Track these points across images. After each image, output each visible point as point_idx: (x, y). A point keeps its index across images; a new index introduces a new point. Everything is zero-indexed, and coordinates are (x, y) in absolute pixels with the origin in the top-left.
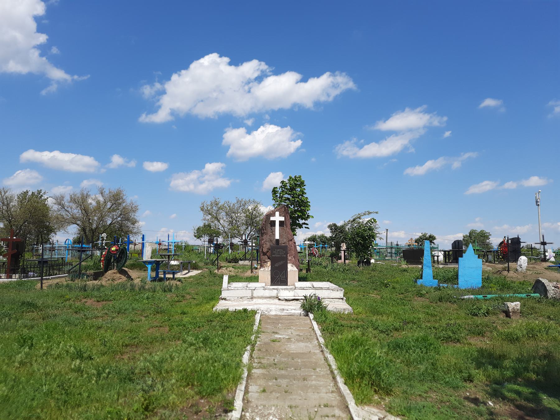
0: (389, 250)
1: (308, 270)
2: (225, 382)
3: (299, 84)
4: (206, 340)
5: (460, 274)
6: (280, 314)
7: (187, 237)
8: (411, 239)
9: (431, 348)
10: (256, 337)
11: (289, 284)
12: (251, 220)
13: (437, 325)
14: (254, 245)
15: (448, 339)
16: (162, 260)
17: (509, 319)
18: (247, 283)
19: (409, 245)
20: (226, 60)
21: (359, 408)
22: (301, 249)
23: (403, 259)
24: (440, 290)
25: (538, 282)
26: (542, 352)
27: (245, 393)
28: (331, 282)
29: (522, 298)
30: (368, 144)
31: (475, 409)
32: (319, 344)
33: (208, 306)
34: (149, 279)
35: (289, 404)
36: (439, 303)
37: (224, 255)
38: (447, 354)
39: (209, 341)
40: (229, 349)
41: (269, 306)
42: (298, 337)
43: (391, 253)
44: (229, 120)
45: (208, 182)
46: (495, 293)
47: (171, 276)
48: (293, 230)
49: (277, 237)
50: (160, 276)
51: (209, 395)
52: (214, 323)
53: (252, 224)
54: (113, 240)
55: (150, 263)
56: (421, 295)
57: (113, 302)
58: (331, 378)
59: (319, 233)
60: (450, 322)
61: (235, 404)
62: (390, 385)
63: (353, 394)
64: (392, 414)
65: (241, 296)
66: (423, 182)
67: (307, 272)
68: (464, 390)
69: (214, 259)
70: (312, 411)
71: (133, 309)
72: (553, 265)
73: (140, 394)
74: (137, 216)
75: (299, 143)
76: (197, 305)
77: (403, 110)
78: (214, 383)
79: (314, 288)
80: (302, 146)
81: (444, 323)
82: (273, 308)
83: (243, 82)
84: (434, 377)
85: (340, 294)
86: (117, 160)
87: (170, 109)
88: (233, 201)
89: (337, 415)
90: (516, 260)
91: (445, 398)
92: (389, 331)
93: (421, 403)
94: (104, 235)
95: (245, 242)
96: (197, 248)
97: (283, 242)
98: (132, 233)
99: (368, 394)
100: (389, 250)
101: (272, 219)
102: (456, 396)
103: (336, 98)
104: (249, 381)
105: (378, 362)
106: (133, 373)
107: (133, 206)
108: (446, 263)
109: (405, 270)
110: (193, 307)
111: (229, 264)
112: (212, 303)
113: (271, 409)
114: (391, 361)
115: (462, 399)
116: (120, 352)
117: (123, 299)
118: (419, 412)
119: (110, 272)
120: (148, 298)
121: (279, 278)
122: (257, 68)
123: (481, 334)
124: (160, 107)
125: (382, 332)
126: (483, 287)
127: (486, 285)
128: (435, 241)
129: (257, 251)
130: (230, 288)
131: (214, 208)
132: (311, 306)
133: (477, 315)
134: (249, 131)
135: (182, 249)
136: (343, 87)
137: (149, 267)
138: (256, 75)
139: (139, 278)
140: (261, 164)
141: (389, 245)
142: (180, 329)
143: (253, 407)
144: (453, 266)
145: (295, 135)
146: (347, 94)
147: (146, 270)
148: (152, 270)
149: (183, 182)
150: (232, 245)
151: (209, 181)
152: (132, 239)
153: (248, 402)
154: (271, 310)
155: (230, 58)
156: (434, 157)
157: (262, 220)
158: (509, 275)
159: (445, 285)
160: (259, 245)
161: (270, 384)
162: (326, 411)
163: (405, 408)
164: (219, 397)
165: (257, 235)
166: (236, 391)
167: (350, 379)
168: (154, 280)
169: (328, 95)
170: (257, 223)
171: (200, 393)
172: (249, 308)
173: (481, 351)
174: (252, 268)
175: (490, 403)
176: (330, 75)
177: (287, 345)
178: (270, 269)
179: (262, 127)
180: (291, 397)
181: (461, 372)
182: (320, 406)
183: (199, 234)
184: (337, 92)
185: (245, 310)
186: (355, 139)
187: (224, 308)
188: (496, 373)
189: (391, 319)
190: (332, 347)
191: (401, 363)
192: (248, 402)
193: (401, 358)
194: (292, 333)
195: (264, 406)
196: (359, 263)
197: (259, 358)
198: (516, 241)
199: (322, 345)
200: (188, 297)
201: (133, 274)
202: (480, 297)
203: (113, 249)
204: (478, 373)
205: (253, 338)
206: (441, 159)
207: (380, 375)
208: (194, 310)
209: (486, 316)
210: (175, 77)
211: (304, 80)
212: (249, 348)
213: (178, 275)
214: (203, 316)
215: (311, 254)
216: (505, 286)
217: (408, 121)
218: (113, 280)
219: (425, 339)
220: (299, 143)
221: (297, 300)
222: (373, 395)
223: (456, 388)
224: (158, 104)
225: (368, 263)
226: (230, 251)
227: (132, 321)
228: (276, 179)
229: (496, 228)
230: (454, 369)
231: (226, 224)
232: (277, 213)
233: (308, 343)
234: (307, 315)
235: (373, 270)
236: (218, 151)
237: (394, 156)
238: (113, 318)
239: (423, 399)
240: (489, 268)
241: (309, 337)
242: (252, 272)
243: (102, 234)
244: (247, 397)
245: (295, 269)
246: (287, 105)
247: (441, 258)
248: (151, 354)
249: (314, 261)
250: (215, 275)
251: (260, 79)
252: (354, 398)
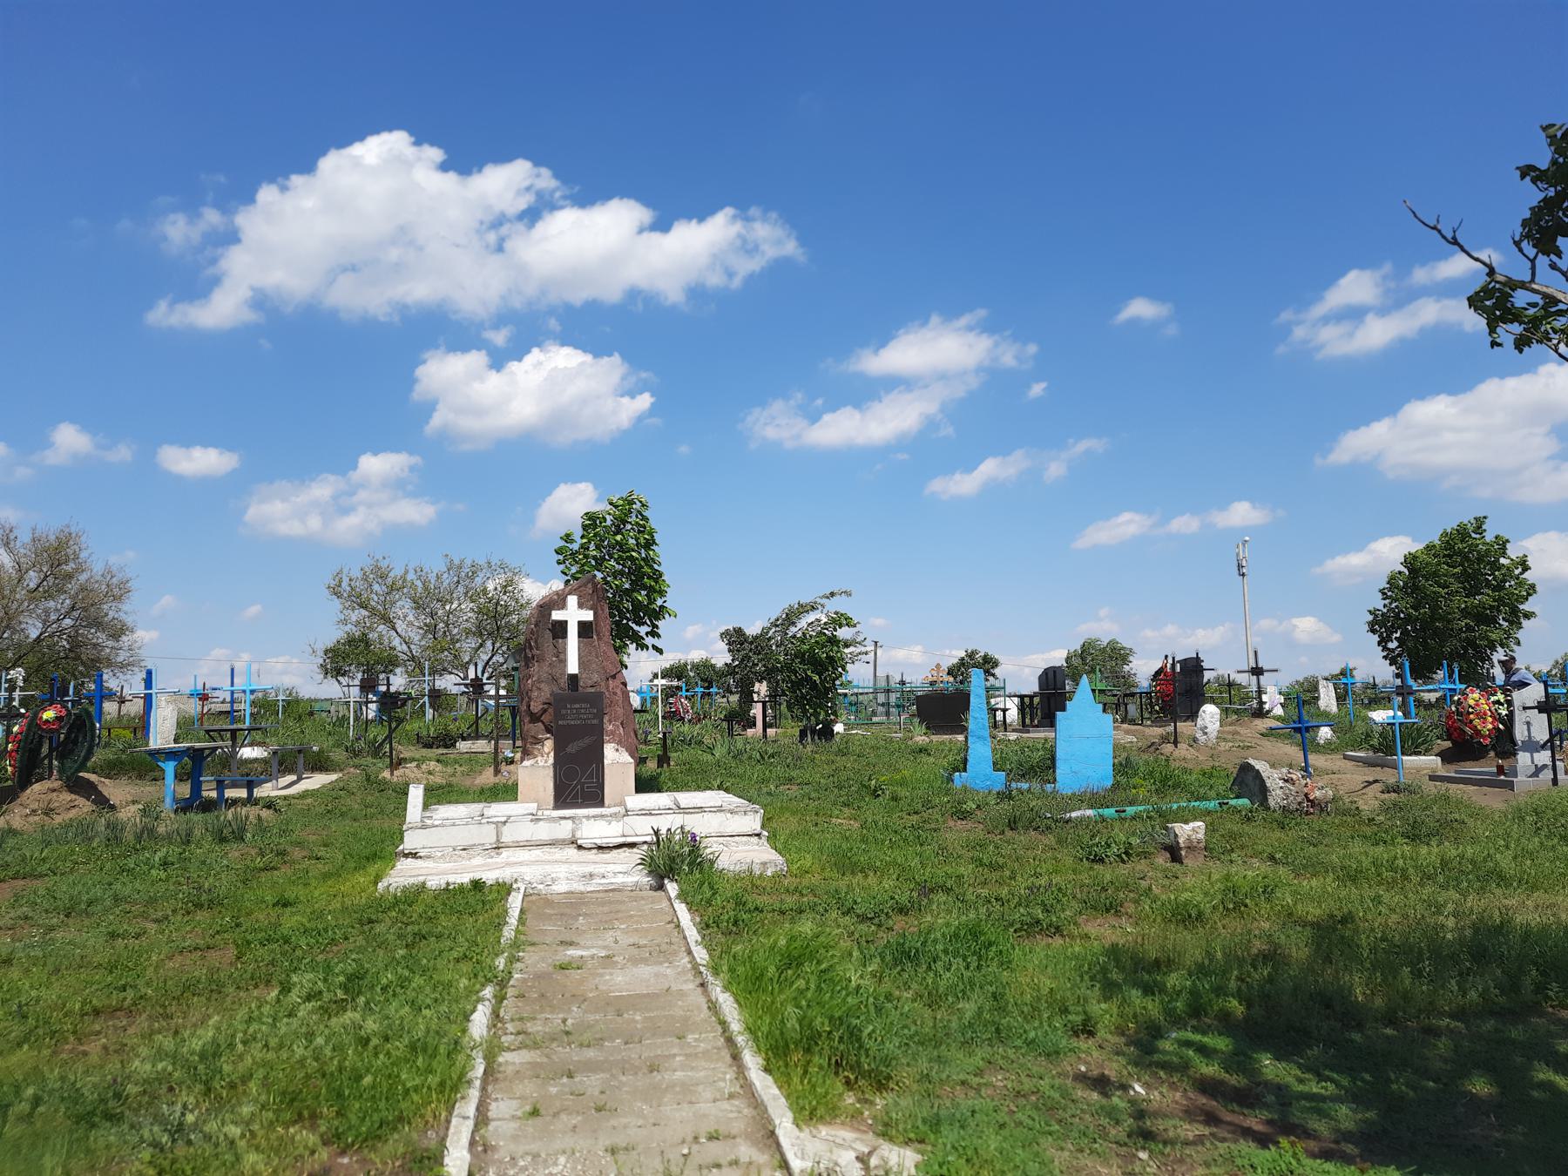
0: (881, 698)
1: (663, 760)
2: (416, 1098)
3: (646, 235)
4: (355, 983)
5: (1059, 754)
6: (582, 888)
7: (295, 672)
8: (938, 666)
9: (991, 954)
10: (513, 960)
11: (607, 802)
12: (493, 619)
13: (1004, 892)
14: (503, 692)
15: (1031, 928)
16: (212, 744)
17: (1177, 866)
18: (481, 805)
19: (932, 683)
20: (435, 154)
21: (805, 1134)
22: (644, 701)
23: (916, 720)
24: (1010, 797)
25: (1246, 769)
26: (1258, 946)
27: (476, 1125)
28: (727, 790)
29: (1209, 813)
30: (834, 410)
31: (1102, 1107)
32: (695, 966)
33: (361, 879)
34: (168, 803)
35: (608, 1143)
36: (1009, 833)
37: (412, 726)
38: (1030, 966)
39: (366, 982)
40: (428, 1001)
41: (548, 868)
42: (635, 951)
43: (886, 705)
44: (440, 328)
45: (368, 509)
46: (1145, 801)
47: (242, 793)
48: (619, 650)
49: (573, 667)
50: (205, 794)
51: (365, 1140)
52: (379, 928)
53: (495, 634)
54: (47, 689)
55: (170, 755)
56: (964, 815)
57: (49, 881)
58: (728, 1058)
59: (696, 656)
60: (1038, 882)
61: (447, 1160)
62: (887, 1061)
63: (787, 1097)
64: (891, 1140)
65: (465, 843)
66: (1118, 518)
67: (660, 765)
68: (1072, 1058)
69: (380, 739)
70: (674, 1156)
71: (117, 899)
72: (1279, 724)
73: (146, 1155)
74: (127, 611)
75: (644, 401)
76: (326, 876)
77: (925, 323)
78: (382, 1105)
79: (680, 809)
80: (653, 411)
81: (1021, 885)
82: (562, 874)
83: (482, 223)
84: (998, 1031)
85: (753, 822)
86: (69, 439)
87: (252, 289)
88: (435, 566)
89: (744, 1159)
90: (1193, 715)
91: (1028, 1084)
92: (883, 917)
93: (966, 1102)
94: (18, 674)
95: (477, 685)
96: (326, 706)
97: (590, 683)
98: (110, 663)
99: (827, 1093)
100: (881, 698)
101: (557, 615)
102: (1053, 1077)
103: (750, 279)
104: (490, 1088)
105: (856, 1001)
106: (118, 1096)
107: (114, 580)
108: (1024, 726)
109: (923, 750)
110: (314, 883)
111: (425, 752)
112: (372, 869)
113: (555, 1164)
114: (889, 997)
115: (1069, 1082)
116: (74, 1032)
117: (82, 869)
118: (962, 1127)
119: (36, 787)
120: (165, 864)
121: (579, 785)
122: (527, 183)
123: (1113, 908)
124: (216, 281)
125: (863, 918)
126: (1116, 786)
127: (1123, 780)
128: (997, 671)
129: (514, 711)
130: (429, 822)
131: (376, 587)
132: (673, 860)
133: (1102, 861)
134: (498, 361)
135: (277, 712)
136: (770, 252)
137: (169, 767)
138: (523, 203)
139: (134, 802)
140: (529, 459)
141: (882, 684)
142: (273, 951)
143: (501, 1162)
144: (1042, 735)
145: (633, 379)
146: (780, 267)
147: (159, 778)
148: (179, 777)
149: (287, 511)
150: (436, 696)
151: (370, 506)
152: (112, 683)
153: (485, 1151)
154: (553, 880)
155: (446, 152)
156: (1001, 449)
157: (527, 621)
158: (1177, 753)
159: (1025, 786)
160: (519, 693)
161: (553, 1090)
162: (715, 1150)
163: (924, 1121)
164: (394, 1145)
165: (511, 664)
166: (448, 1122)
167: (778, 1054)
168: (184, 806)
169: (730, 274)
170: (514, 631)
171: (338, 1136)
172: (489, 877)
173: (1114, 952)
174: (497, 762)
175: (1138, 1088)
176: (734, 217)
177: (602, 975)
178: (551, 760)
179: (535, 351)
180: (613, 1122)
181: (1065, 1011)
182: (696, 1138)
183: (336, 662)
184: (752, 265)
185: (477, 885)
186: (799, 395)
187: (412, 881)
188: (1152, 1008)
189: (888, 884)
190: (732, 970)
191: (914, 1000)
192: (485, 1151)
193: (914, 986)
194: (616, 942)
195: (536, 1156)
196: (803, 734)
197: (521, 1019)
198: (1193, 667)
199: (702, 969)
200: (297, 853)
201: (115, 790)
202: (1110, 812)
203: (49, 715)
204: (1106, 1012)
205: (501, 962)
206: (1019, 454)
207: (859, 1040)
208: (316, 893)
209: (1123, 862)
210: (267, 194)
211: (662, 225)
212: (488, 992)
213: (265, 791)
214: (344, 909)
215: (672, 716)
216: (1168, 783)
217: (937, 353)
218: (48, 812)
219: (975, 932)
220: (644, 401)
221: (632, 845)
222: (841, 1095)
223: (1053, 1054)
224: (210, 271)
225: (827, 733)
226: (429, 713)
227: (113, 936)
228: (573, 503)
229: (1149, 633)
230: (1050, 1005)
231: (415, 635)
232: (572, 600)
233: (667, 966)
234: (661, 887)
235: (842, 753)
236: (397, 416)
237: (902, 443)
238: (52, 929)
239: (972, 1093)
240: (1129, 737)
241: (664, 947)
242: (497, 772)
243: (8, 669)
244: (483, 1137)
246: (612, 293)
247: (1013, 714)
248: (176, 1033)
249: (680, 733)
250: (383, 787)
251: (531, 216)
252: (791, 1108)
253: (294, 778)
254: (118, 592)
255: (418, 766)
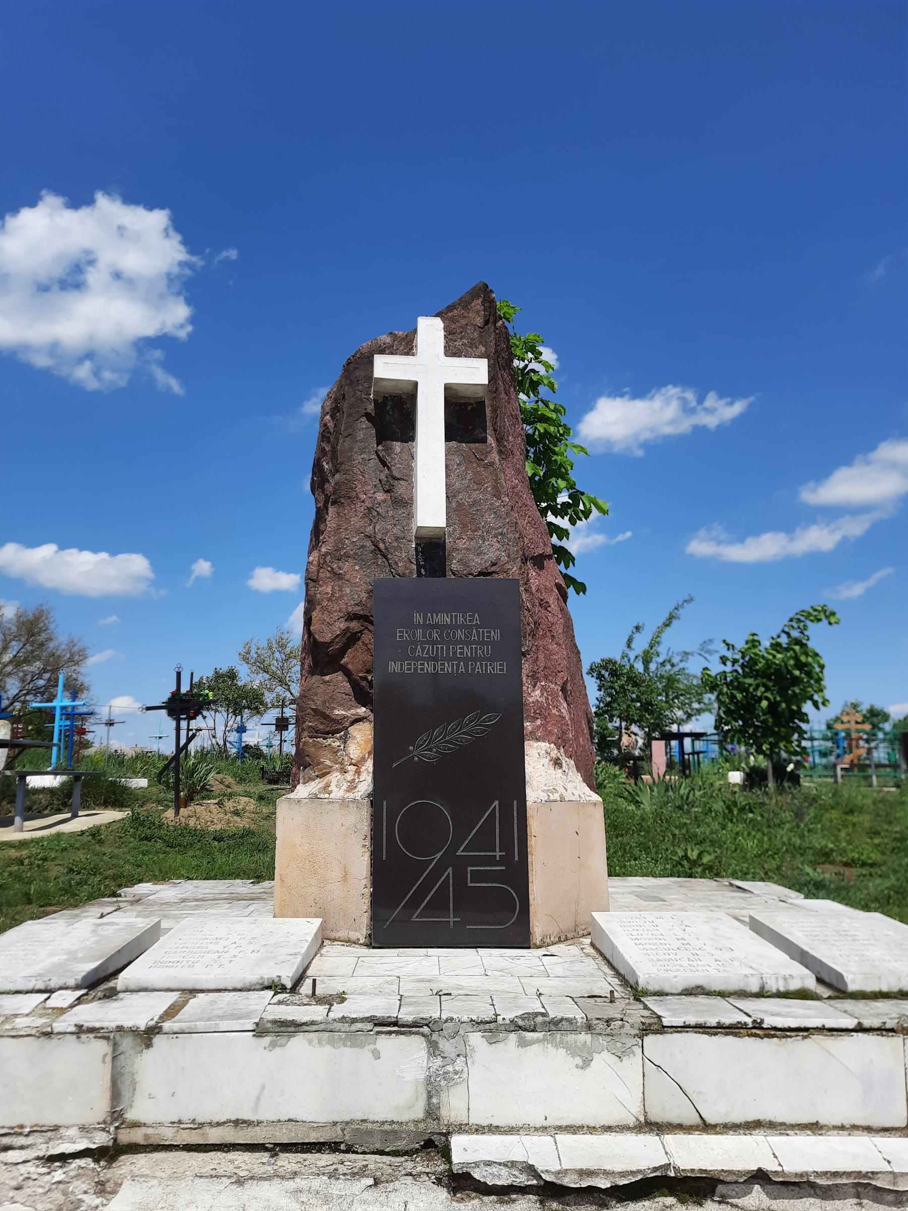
11: (538, 927)
49: (430, 510)
101: (388, 368)
131: (277, 655)
178: (366, 784)
245: (576, 787)
253: (69, 815)
254: (76, 657)
255: (220, 804)
